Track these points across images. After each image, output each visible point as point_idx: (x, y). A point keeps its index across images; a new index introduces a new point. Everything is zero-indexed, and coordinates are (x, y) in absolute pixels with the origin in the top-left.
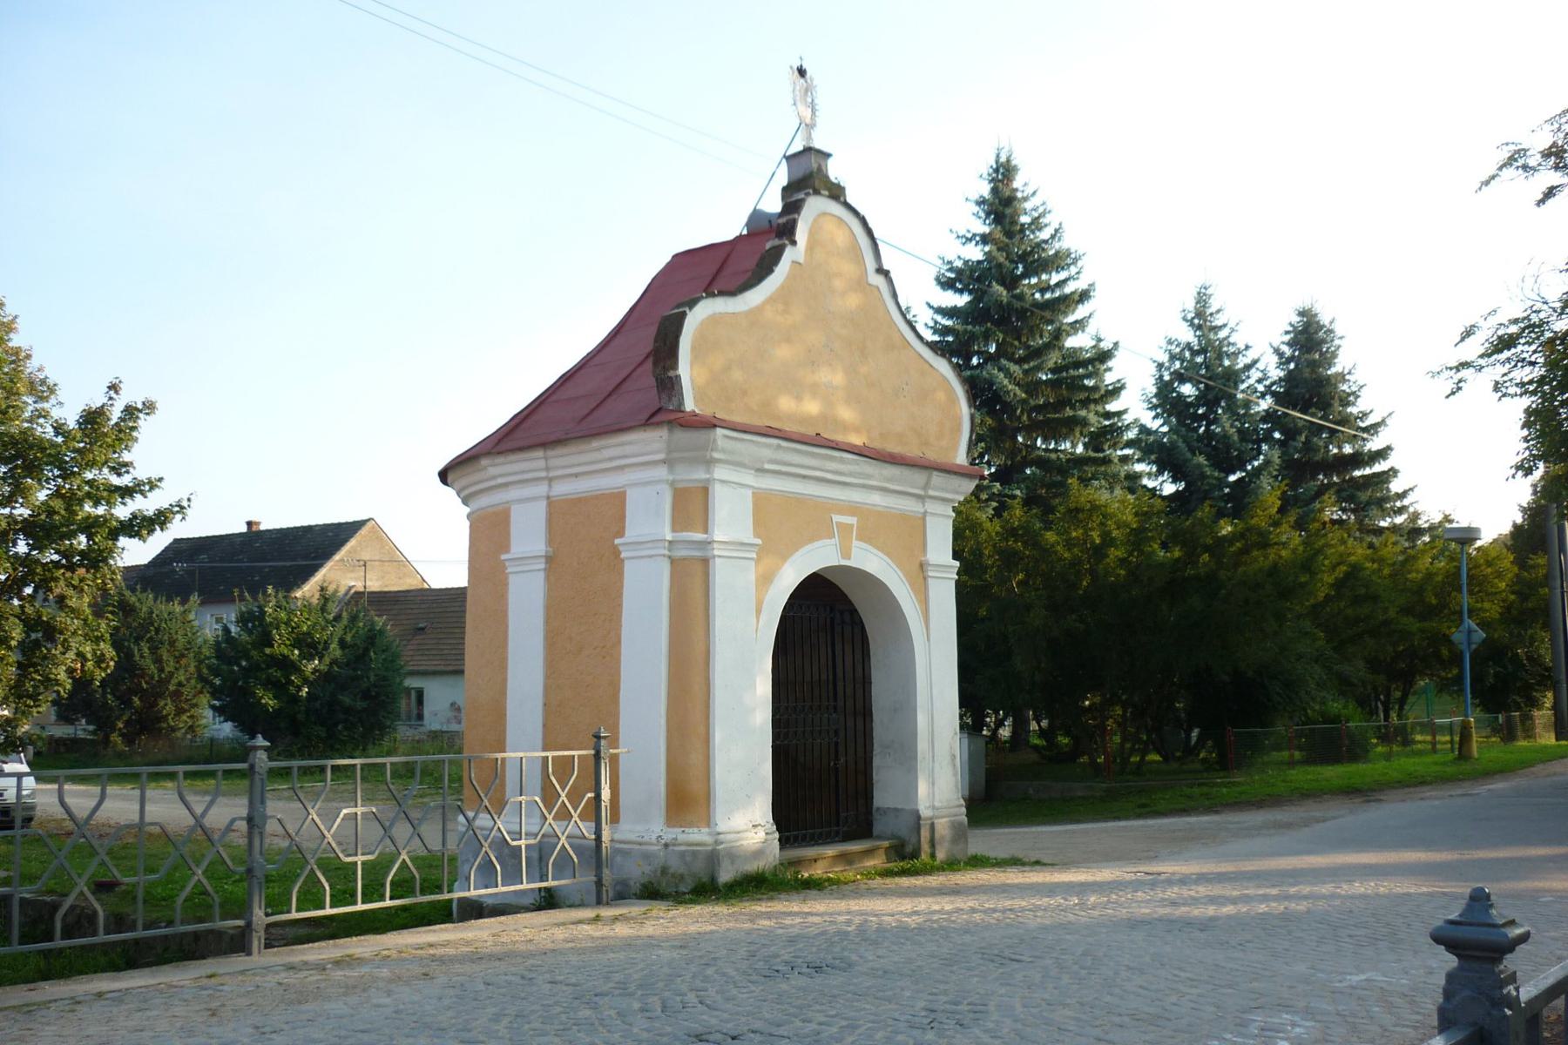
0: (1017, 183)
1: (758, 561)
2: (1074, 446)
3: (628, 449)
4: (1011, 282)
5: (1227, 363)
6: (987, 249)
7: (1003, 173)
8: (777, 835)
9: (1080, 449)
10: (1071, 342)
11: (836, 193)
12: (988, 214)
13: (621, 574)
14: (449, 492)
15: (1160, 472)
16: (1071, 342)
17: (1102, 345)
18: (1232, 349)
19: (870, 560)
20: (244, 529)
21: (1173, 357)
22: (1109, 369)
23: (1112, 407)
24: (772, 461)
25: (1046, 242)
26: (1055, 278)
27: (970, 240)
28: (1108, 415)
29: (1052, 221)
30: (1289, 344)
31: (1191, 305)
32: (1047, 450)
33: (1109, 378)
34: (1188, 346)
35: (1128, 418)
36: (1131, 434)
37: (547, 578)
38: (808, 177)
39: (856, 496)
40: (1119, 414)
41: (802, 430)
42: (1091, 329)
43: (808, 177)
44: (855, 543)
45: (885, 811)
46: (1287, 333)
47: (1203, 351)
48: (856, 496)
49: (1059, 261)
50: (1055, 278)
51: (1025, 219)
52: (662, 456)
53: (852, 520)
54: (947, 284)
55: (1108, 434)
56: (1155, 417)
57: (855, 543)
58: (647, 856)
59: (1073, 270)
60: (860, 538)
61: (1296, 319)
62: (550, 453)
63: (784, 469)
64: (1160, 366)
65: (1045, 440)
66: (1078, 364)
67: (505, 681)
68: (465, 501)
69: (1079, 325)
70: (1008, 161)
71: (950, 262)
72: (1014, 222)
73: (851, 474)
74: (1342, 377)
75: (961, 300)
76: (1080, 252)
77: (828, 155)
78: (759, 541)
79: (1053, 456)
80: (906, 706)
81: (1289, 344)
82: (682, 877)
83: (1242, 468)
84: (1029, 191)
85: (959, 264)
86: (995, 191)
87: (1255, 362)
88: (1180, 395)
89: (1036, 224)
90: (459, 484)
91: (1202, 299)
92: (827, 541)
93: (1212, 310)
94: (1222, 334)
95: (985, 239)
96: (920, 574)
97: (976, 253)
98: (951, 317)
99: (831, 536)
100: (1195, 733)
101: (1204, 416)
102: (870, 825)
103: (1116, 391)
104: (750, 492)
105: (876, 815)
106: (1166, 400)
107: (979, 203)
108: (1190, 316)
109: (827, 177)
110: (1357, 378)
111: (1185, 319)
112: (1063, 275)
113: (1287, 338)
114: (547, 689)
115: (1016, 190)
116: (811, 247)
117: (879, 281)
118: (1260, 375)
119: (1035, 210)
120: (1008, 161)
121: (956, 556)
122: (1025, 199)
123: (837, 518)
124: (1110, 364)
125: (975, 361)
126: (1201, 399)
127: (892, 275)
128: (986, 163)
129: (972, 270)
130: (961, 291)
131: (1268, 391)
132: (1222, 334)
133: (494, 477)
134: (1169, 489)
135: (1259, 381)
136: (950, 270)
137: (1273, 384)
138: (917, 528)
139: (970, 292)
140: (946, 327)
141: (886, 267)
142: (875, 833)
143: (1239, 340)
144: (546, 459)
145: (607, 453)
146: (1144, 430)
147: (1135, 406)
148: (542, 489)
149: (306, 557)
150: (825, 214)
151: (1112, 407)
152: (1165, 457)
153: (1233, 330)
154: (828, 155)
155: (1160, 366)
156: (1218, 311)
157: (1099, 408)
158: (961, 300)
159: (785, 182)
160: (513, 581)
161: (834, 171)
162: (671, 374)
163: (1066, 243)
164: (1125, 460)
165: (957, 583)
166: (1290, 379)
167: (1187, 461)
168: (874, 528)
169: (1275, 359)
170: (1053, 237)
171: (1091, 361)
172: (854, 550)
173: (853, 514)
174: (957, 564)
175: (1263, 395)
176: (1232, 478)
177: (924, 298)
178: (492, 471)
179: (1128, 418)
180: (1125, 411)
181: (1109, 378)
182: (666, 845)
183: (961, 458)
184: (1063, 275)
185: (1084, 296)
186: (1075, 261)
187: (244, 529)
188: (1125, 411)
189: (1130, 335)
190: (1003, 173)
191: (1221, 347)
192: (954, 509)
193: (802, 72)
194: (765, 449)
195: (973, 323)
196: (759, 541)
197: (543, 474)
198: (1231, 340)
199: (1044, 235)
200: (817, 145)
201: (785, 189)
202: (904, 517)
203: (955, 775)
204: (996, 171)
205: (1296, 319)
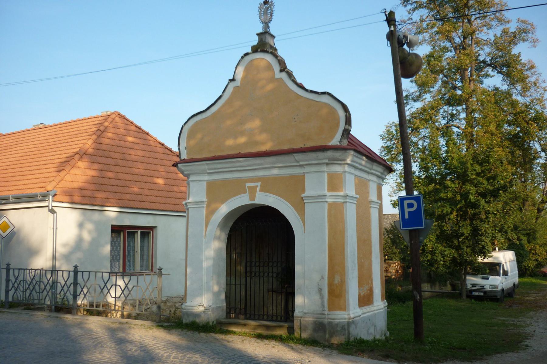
92: (242, 195)
99: (245, 192)
117: (284, 75)
123: (248, 185)
161: (255, 41)
168: (268, 185)
202: (292, 177)
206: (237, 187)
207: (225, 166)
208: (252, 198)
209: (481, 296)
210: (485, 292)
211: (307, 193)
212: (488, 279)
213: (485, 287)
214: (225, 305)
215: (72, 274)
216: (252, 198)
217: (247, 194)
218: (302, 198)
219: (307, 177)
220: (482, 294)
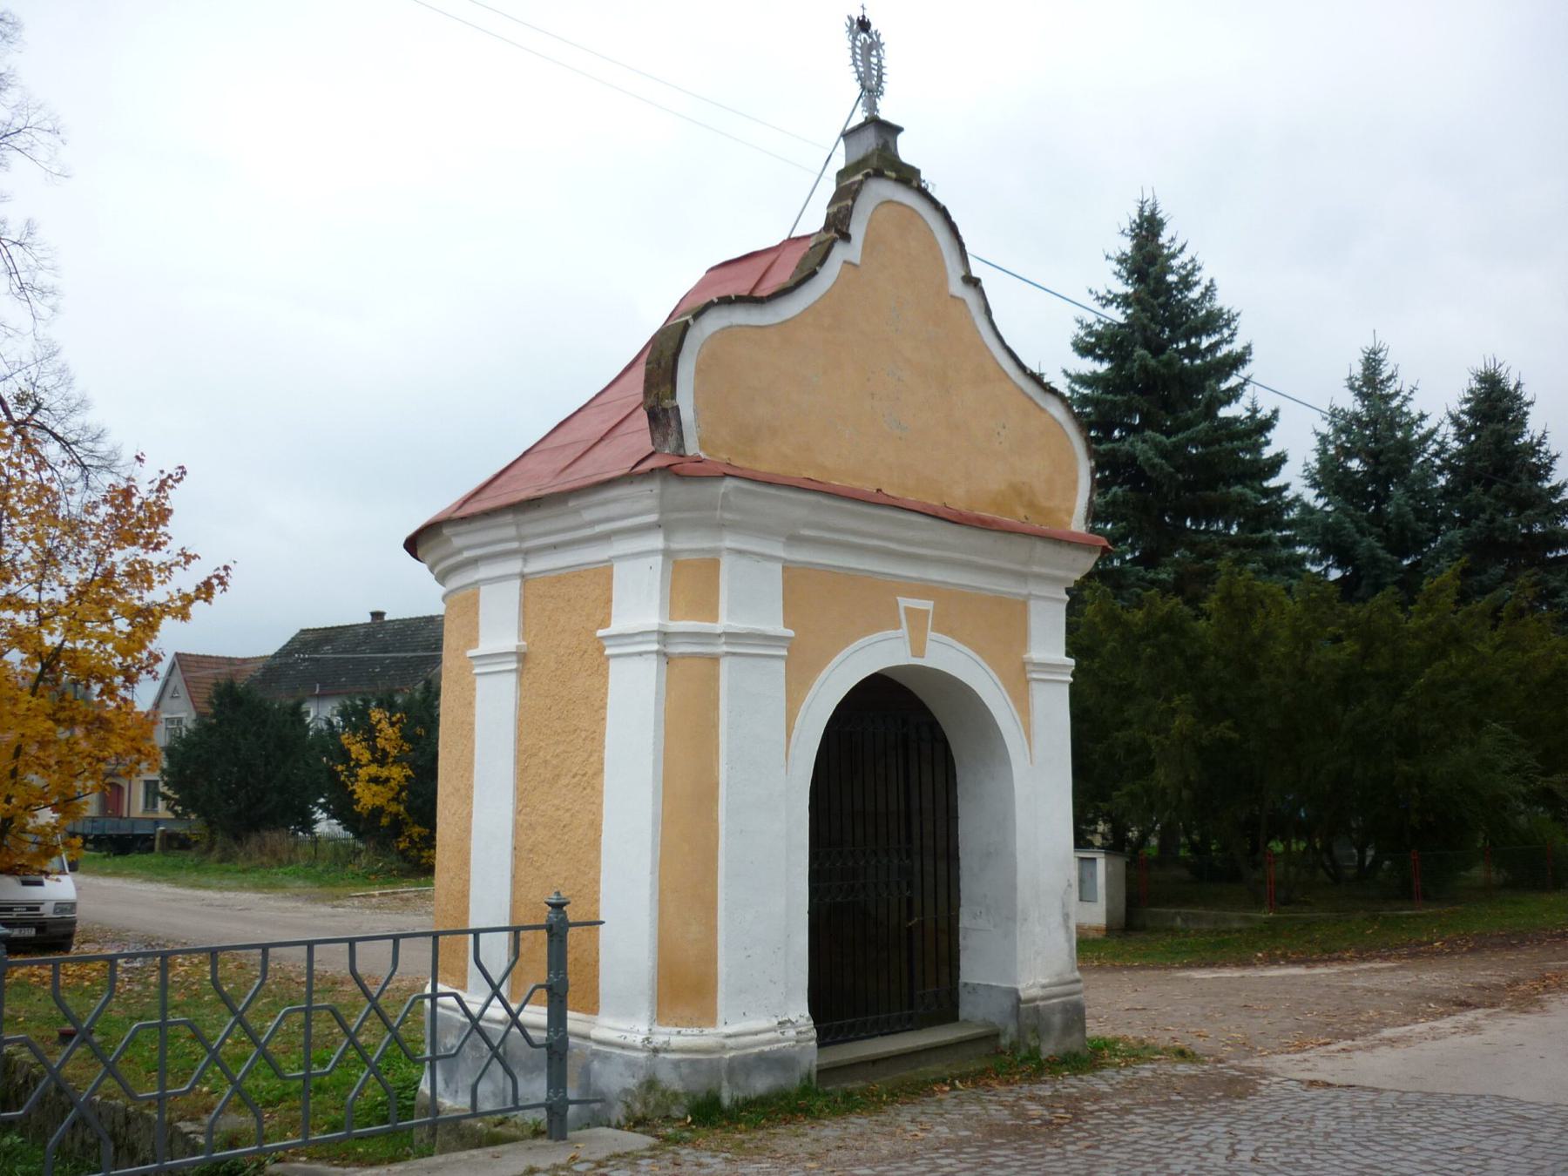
0: (1164, 239)
1: (787, 659)
2: (1228, 526)
3: (614, 509)
4: (1158, 349)
5: (1399, 434)
6: (1129, 311)
7: (1148, 228)
8: (814, 1033)
9: (1234, 530)
10: (1224, 412)
11: (908, 177)
12: (1131, 273)
13: (605, 676)
14: (421, 569)
15: (1324, 556)
16: (1224, 412)
17: (1259, 416)
18: (1405, 420)
19: (949, 656)
20: (368, 619)
21: (1339, 430)
22: (1268, 443)
23: (1272, 483)
24: (808, 525)
25: (1195, 301)
26: (1205, 342)
27: (1110, 302)
28: (1267, 493)
29: (1203, 277)
30: (1469, 413)
31: (1358, 370)
32: (1197, 531)
33: (1268, 452)
34: (1356, 417)
35: (1288, 495)
36: (1293, 514)
37: (520, 682)
38: (876, 156)
39: (934, 574)
40: (1280, 490)
41: (857, 484)
42: (1245, 401)
43: (876, 156)
44: (931, 635)
45: (975, 988)
46: (1467, 401)
47: (1373, 422)
48: (934, 574)
49: (1214, 321)
50: (1205, 342)
51: (1171, 278)
52: (653, 518)
53: (927, 605)
54: (1084, 350)
55: (1272, 510)
56: (1318, 496)
57: (931, 635)
58: (630, 1064)
59: (1226, 332)
60: (936, 629)
61: (1475, 385)
62: (522, 518)
63: (827, 535)
64: (1324, 439)
65: (1196, 521)
66: (1233, 436)
67: (470, 815)
68: (442, 578)
69: (1234, 394)
70: (1153, 214)
71: (1089, 326)
72: (1161, 279)
73: (923, 544)
74: (1532, 449)
75: (1102, 368)
76: (1234, 312)
77: (898, 130)
78: (791, 633)
79: (1204, 538)
80: (1001, 853)
81: (1469, 413)
82: (676, 1095)
83: (1418, 551)
84: (1177, 246)
85: (1098, 327)
86: (1138, 247)
87: (1433, 432)
88: (1347, 469)
89: (1186, 283)
90: (431, 558)
91: (1372, 363)
92: (890, 633)
93: (1384, 376)
94: (1395, 403)
95: (1125, 301)
96: (1019, 681)
97: (1117, 315)
98: (1089, 386)
99: (897, 626)
100: (1370, 853)
101: (1374, 494)
102: (955, 1006)
103: (1279, 461)
104: (779, 567)
105: (964, 997)
106: (1329, 476)
107: (1120, 261)
108: (1357, 384)
109: (897, 156)
110: (1552, 446)
111: (1352, 387)
112: (1215, 338)
113: (1466, 407)
114: (517, 828)
115: (1163, 246)
116: (868, 246)
117: (969, 295)
118: (1435, 447)
119: (1184, 266)
120: (1153, 214)
121: (1073, 649)
122: (1173, 256)
123: (904, 602)
124: (1269, 435)
125: (1116, 433)
126: (1371, 476)
127: (984, 284)
128: (1129, 215)
129: (1114, 336)
130: (1100, 359)
131: (1447, 466)
132: (1395, 403)
133: (460, 551)
134: (1335, 574)
135: (1437, 454)
136: (1090, 334)
137: (1452, 457)
138: (1015, 615)
139: (1111, 360)
140: (1084, 396)
141: (975, 274)
142: (963, 1014)
143: (1414, 408)
144: (518, 526)
145: (588, 516)
146: (1306, 508)
147: (1295, 480)
148: (515, 566)
149: (426, 649)
150: (890, 202)
151: (1272, 483)
152: (1333, 544)
153: (1406, 399)
154: (898, 130)
155: (1324, 439)
156: (1390, 378)
157: (1256, 484)
158: (1102, 368)
159: (842, 166)
160: (482, 685)
161: (907, 150)
162: (667, 403)
163: (1222, 301)
164: (1288, 542)
165: (1072, 685)
166: (1468, 454)
167: (1355, 543)
168: (956, 613)
169: (1452, 430)
170: (1203, 295)
171: (1248, 434)
172: (930, 646)
173: (928, 598)
174: (1072, 662)
175: (1440, 471)
176: (1406, 562)
177: (1060, 362)
178: (458, 542)
179: (1288, 495)
180: (1286, 487)
181: (1268, 452)
182: (656, 1051)
183: (1077, 523)
184: (1215, 338)
185: (1238, 360)
186: (1228, 325)
187: (368, 619)
188: (1286, 487)
189: (1292, 395)
190: (1148, 228)
191: (1393, 418)
192: (1068, 591)
193: (864, 25)
194: (797, 508)
195: (1115, 393)
196: (791, 633)
197: (515, 545)
198: (1405, 409)
199: (1195, 293)
200: (884, 115)
201: (841, 175)
202: (1000, 601)
203: (1069, 940)
204: (1140, 226)
205: (1475, 385)
206: (871, 606)
207: (874, 528)
208: (918, 650)
209: (30, 939)
210: (41, 925)
211: (616, 627)
212: (40, 884)
213: (43, 909)
214: (570, 1014)
215: (537, 943)
216: (918, 650)
217: (904, 631)
218: (1024, 664)
219: (619, 570)
220: (32, 932)
